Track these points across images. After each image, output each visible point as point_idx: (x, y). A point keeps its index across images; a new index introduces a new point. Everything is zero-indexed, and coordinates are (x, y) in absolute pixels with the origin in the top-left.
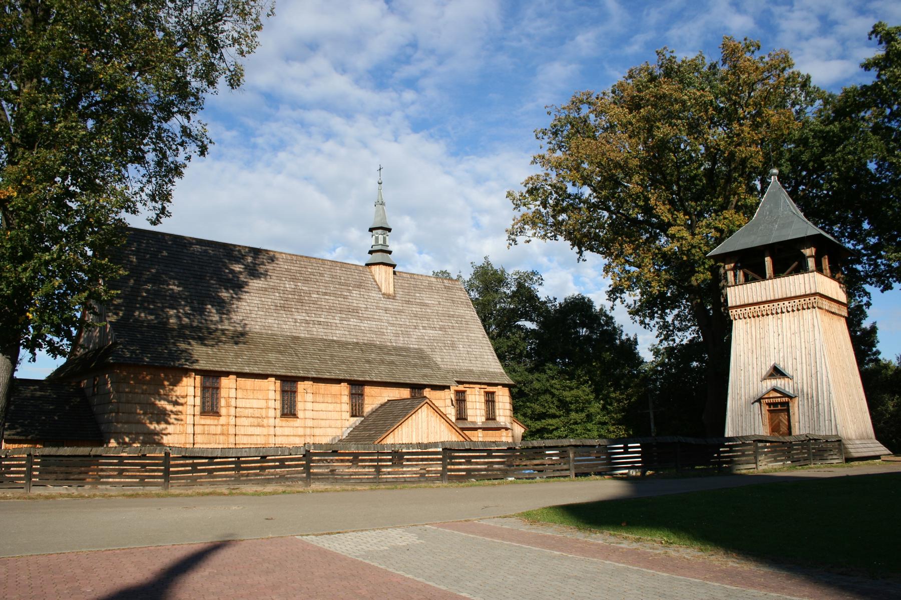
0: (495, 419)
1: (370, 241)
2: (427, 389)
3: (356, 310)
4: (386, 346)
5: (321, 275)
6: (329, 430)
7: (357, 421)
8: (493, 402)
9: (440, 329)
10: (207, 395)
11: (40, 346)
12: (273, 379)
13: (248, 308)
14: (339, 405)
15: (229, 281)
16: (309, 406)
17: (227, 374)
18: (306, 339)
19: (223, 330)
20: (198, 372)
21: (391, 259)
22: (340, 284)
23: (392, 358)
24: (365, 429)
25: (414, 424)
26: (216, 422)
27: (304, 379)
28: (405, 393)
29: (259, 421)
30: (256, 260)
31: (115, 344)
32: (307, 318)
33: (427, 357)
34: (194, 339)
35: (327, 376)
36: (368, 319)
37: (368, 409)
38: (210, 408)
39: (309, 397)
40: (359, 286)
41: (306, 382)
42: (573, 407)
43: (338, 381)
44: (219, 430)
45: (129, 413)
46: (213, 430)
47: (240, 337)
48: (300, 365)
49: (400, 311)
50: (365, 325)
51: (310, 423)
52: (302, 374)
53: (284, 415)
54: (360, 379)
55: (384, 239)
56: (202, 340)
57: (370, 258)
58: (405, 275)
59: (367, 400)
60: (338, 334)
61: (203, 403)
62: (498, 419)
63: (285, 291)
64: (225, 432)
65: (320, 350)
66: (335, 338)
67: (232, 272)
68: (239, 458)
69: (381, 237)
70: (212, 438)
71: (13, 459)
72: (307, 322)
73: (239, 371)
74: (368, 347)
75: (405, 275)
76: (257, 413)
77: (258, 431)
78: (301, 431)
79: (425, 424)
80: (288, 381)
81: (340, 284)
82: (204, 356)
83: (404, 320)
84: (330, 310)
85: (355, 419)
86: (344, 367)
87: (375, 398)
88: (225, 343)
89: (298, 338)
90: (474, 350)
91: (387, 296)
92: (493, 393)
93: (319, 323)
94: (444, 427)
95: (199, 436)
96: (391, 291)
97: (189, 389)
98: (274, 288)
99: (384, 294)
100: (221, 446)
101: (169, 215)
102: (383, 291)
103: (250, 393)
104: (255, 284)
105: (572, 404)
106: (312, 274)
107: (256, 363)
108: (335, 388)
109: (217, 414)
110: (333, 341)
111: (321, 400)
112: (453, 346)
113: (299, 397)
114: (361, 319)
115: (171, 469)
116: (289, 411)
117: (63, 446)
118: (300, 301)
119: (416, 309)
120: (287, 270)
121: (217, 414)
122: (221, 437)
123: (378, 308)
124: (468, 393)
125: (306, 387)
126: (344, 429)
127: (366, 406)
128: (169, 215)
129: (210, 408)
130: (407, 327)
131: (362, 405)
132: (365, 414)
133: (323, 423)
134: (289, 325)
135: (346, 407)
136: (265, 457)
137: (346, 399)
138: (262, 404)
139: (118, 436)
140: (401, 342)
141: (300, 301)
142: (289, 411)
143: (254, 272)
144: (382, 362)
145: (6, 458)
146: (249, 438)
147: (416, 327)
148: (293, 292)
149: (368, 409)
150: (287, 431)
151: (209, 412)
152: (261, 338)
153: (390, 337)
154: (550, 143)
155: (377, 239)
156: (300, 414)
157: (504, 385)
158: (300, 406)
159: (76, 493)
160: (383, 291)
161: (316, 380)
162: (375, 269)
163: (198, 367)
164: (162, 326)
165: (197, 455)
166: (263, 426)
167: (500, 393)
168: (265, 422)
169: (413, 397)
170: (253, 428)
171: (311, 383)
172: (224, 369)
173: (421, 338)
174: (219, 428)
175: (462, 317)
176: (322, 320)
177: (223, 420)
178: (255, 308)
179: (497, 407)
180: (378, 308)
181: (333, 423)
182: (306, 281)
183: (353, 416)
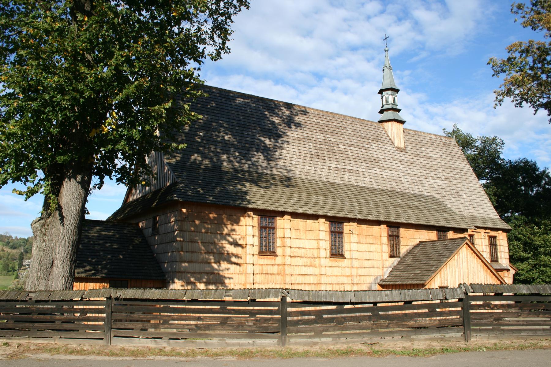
0: (497, 261)
1: (378, 102)
2: (451, 232)
3: (376, 161)
4: (406, 193)
5: (345, 128)
6: (372, 270)
7: (395, 261)
8: (495, 245)
9: (446, 179)
10: (263, 235)
11: (109, 174)
12: (323, 220)
13: (287, 155)
14: (379, 246)
15: (269, 130)
16: (355, 246)
17: (282, 214)
18: (339, 184)
19: (271, 175)
20: (257, 211)
21: (402, 116)
22: (361, 137)
23: (415, 203)
24: (406, 269)
25: (456, 264)
26: (272, 262)
27: (350, 220)
28: (432, 235)
29: (312, 261)
30: (292, 114)
31: (174, 184)
32: (339, 166)
33: (439, 204)
34: (247, 181)
35: (369, 218)
36: (388, 168)
37: (403, 250)
38: (267, 249)
39: (354, 238)
40: (377, 140)
41: (351, 224)
42: (542, 250)
43: (378, 223)
44: (275, 270)
45: (192, 252)
46: (270, 269)
47: (287, 181)
48: (344, 207)
49: (412, 163)
50: (386, 174)
51: (356, 263)
52: (348, 215)
53: (333, 256)
54: (398, 221)
55: (394, 99)
56: (255, 182)
57: (381, 117)
58: (411, 132)
59: (402, 242)
60: (365, 182)
61: (261, 243)
62: (500, 260)
63: (317, 141)
64: (282, 272)
65: (356, 195)
66: (364, 185)
67: (273, 123)
68: (375, 303)
69: (391, 98)
70: (270, 278)
71: (89, 302)
72: (339, 170)
73: (294, 211)
74: (392, 193)
75: (411, 132)
76: (309, 253)
77: (310, 270)
78: (348, 271)
79: (465, 265)
80: (335, 222)
81: (361, 137)
82: (258, 197)
83: (416, 171)
84: (356, 159)
85: (393, 259)
86: (380, 210)
87: (410, 239)
88: (276, 185)
89: (333, 184)
90: (473, 201)
91: (399, 149)
92: (495, 237)
93: (349, 171)
94: (480, 267)
95: (258, 276)
96: (402, 146)
97: (247, 228)
98: (308, 139)
99: (396, 148)
100: (278, 286)
101: (228, 51)
102: (396, 145)
103: (303, 233)
104: (293, 134)
105: (541, 247)
106: (337, 127)
107: (306, 204)
108: (375, 229)
109: (273, 254)
110: (363, 187)
111: (364, 241)
112: (458, 195)
113: (346, 238)
114: (382, 168)
115: (289, 318)
116: (337, 253)
117: (151, 288)
118: (331, 151)
119: (423, 161)
120: (317, 123)
121: (273, 254)
122: (278, 277)
123: (394, 159)
124: (475, 237)
125: (351, 228)
126: (385, 269)
127: (401, 247)
128: (228, 51)
129: (267, 249)
130: (420, 177)
131: (398, 245)
132: (401, 255)
133: (366, 264)
134: (324, 171)
135: (386, 248)
136: (410, 302)
137: (385, 240)
138: (314, 244)
139: (182, 275)
140: (416, 190)
141: (331, 151)
142: (337, 253)
143: (290, 122)
144: (409, 207)
145: (82, 301)
146: (303, 277)
147: (426, 177)
148: (325, 142)
149: (403, 250)
150: (336, 271)
151: (266, 252)
152: (304, 182)
153: (407, 186)
154: (524, 17)
155: (387, 99)
156: (347, 254)
157: (504, 230)
158: (346, 246)
159: (168, 349)
160: (396, 145)
161: (361, 222)
162: (387, 125)
163: (256, 207)
164: (217, 168)
165: (323, 300)
166: (315, 266)
167: (501, 238)
168: (317, 262)
169: (439, 239)
170: (306, 268)
171: (356, 224)
172: (280, 209)
173: (432, 187)
174: (276, 267)
175: (461, 169)
176: (351, 168)
177: (279, 260)
178: (294, 155)
179: (499, 251)
180: (394, 159)
181: (375, 263)
182: (333, 133)
183: (391, 256)
